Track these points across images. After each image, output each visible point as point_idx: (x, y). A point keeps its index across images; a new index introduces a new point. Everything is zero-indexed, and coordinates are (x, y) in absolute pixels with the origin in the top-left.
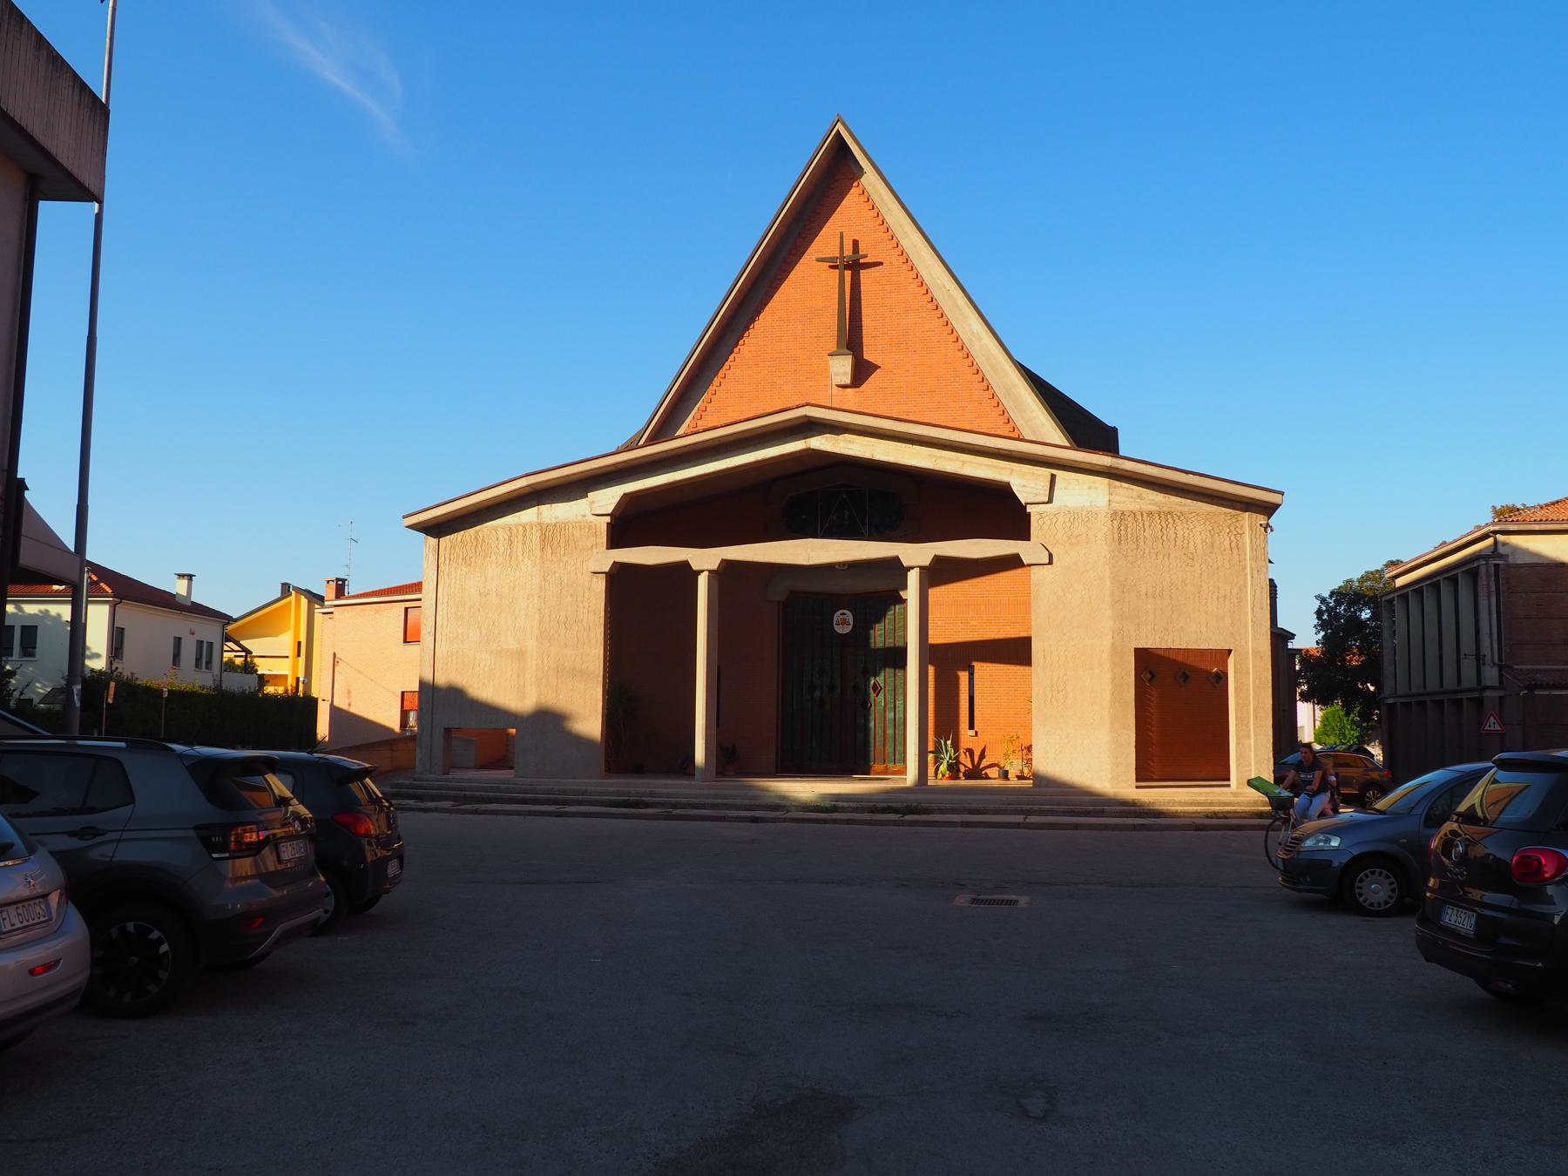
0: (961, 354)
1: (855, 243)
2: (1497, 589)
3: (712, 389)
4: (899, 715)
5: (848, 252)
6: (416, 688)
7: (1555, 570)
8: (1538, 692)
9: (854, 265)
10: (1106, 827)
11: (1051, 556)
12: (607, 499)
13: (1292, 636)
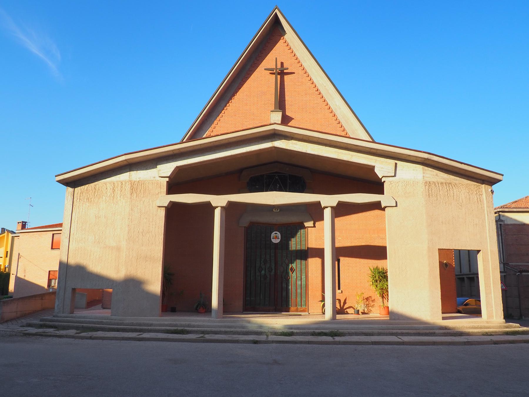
0: (331, 115)
1: (282, 64)
2: (501, 234)
3: (213, 126)
4: (304, 283)
5: (279, 66)
6: (57, 268)
7: (523, 226)
8: (523, 274)
9: (281, 73)
10: (434, 343)
11: (396, 202)
12: (167, 169)
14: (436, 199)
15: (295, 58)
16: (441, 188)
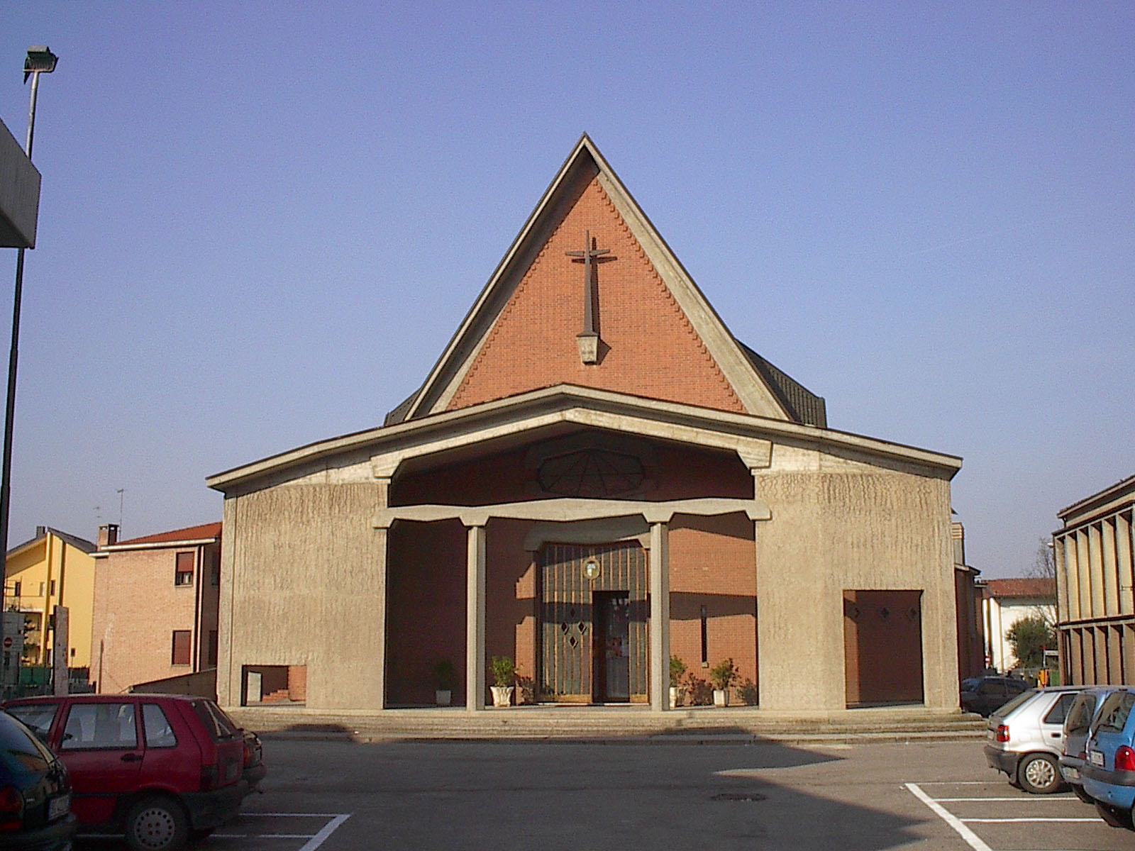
11: (771, 513)
12: (389, 462)
13: (979, 572)
14: (842, 504)
15: (623, 228)
16: (851, 485)
